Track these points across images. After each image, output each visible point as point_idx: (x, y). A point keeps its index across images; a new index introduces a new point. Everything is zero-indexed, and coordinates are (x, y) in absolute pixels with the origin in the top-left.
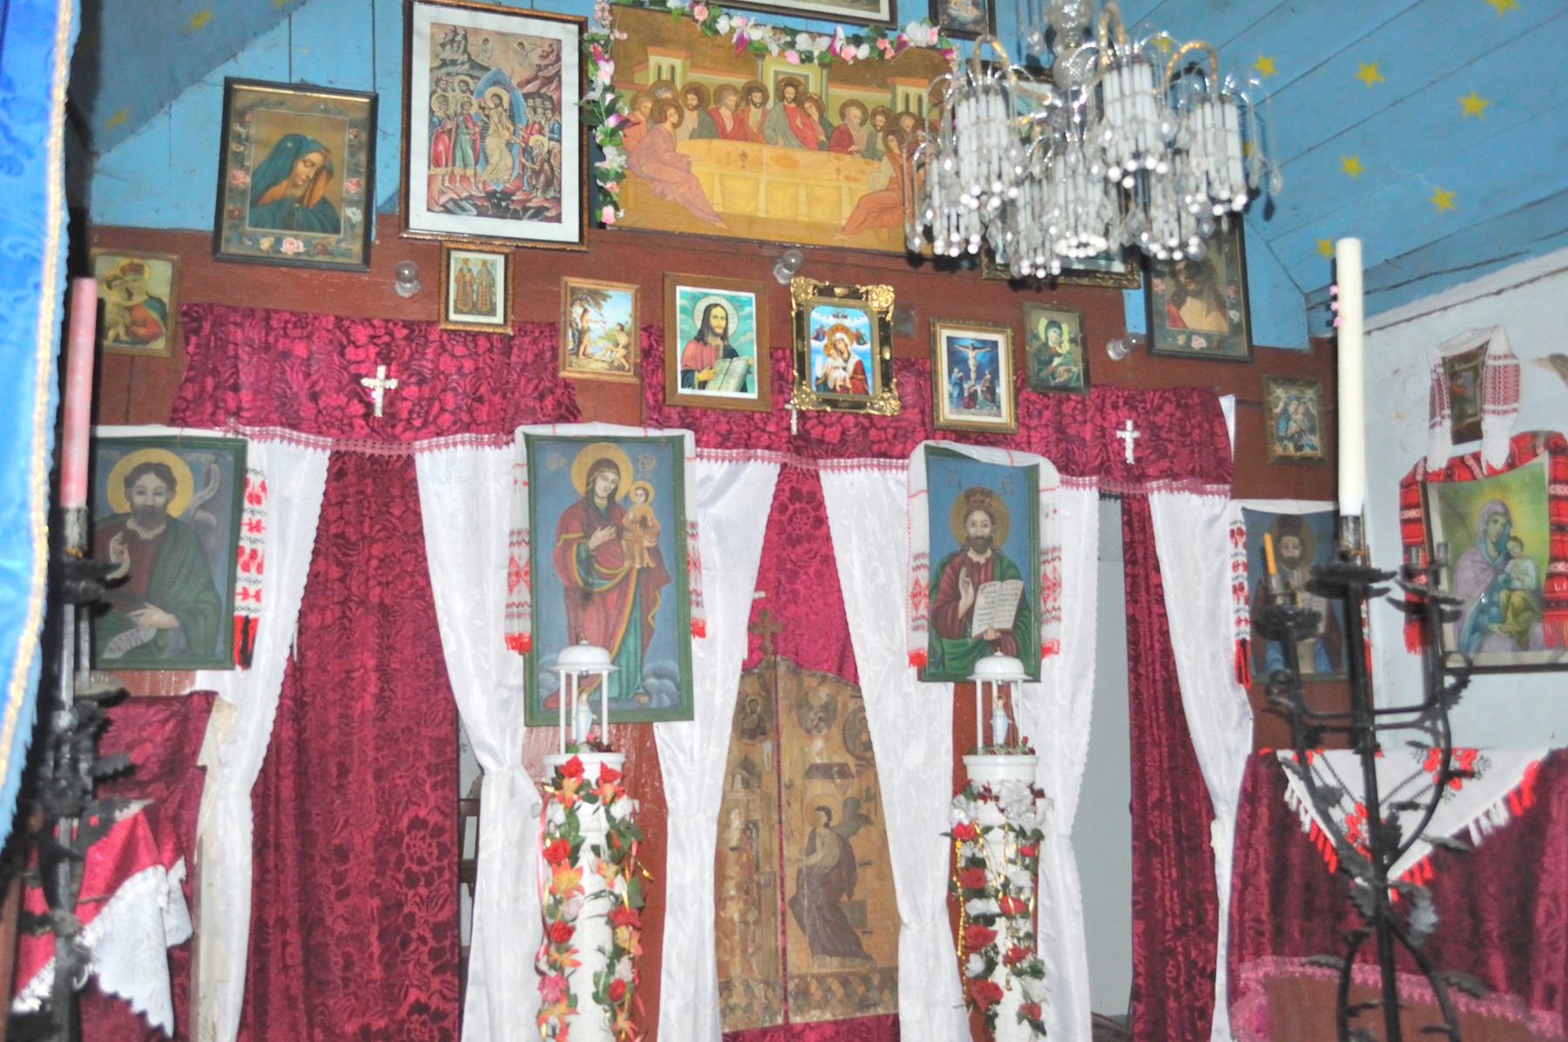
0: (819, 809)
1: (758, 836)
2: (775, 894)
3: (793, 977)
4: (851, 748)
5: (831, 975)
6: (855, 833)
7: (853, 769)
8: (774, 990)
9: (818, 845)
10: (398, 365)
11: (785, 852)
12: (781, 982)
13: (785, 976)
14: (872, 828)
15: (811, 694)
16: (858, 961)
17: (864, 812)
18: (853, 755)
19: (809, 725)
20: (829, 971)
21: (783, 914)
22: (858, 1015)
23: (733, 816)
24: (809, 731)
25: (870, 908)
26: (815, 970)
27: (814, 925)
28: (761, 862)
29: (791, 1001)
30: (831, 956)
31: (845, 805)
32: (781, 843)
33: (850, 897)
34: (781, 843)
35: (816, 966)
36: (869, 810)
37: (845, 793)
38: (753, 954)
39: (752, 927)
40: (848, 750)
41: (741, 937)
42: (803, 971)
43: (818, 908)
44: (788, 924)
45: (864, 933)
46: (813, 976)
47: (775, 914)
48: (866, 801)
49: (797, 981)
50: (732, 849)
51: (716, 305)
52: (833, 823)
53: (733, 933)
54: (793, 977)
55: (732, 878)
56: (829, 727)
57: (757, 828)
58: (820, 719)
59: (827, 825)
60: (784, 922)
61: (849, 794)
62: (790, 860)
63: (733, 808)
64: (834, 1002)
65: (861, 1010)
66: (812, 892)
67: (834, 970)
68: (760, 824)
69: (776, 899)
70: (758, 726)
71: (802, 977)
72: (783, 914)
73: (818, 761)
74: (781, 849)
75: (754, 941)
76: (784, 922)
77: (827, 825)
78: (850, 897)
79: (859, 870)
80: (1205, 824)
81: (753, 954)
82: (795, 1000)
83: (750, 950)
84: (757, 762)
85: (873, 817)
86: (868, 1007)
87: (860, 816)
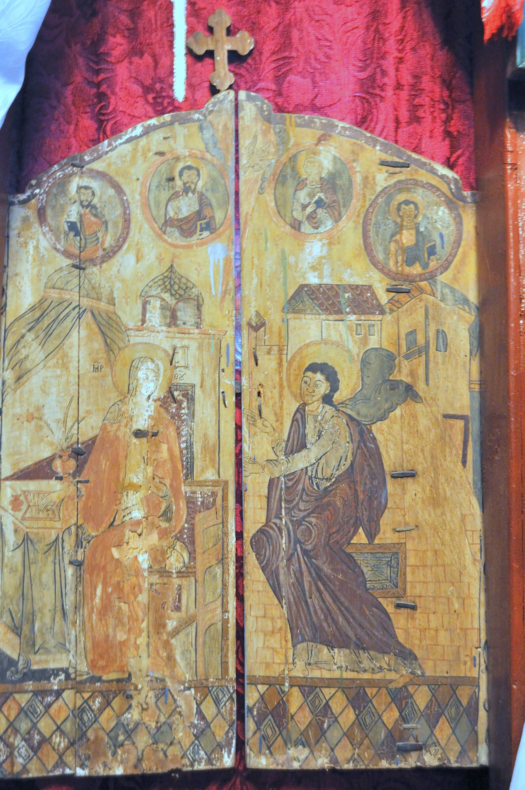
0: (313, 368)
1: (192, 415)
2: (224, 523)
3: (255, 682)
4: (381, 256)
5: (330, 683)
6: (382, 418)
7: (384, 298)
8: (217, 702)
9: (311, 437)
10: (203, 758)
11: (245, 447)
12: (232, 687)
13: (240, 675)
14: (419, 407)
15: (302, 158)
16: (385, 660)
17: (404, 377)
18: (383, 270)
19: (298, 215)
20: (327, 675)
21: (240, 560)
22: (384, 764)
23: (141, 374)
24: (296, 226)
25: (411, 560)
26: (299, 671)
27: (299, 582)
28: (198, 464)
29: (250, 725)
30: (331, 646)
31: (365, 363)
32: (238, 427)
33: (371, 536)
34: (238, 427)
35: (300, 664)
36: (412, 374)
37: (365, 341)
38: (176, 632)
39: (176, 582)
40: (374, 262)
41: (151, 598)
42: (275, 671)
43: (305, 552)
44: (248, 581)
45: (398, 606)
46: (294, 682)
47: (222, 561)
48: (407, 357)
49: (262, 688)
50: (139, 434)
51: (199, 175)
52: (337, 397)
53: (136, 589)
54: (255, 682)
55: (136, 488)
56: (337, 220)
57: (191, 399)
58: (319, 203)
59: (327, 399)
60: (240, 575)
61: (373, 342)
62: (254, 461)
63: (143, 359)
64: (334, 734)
65: (392, 757)
66: (297, 524)
67: (337, 674)
68: (198, 391)
69: (226, 534)
70: (199, 215)
71: (269, 682)
72: (240, 560)
73: (313, 280)
74: (239, 440)
75: (178, 609)
76: (240, 575)
77: (327, 399)
78: (371, 536)
79: (391, 486)
80: (515, 723)
81: (176, 632)
82: (258, 724)
83: (171, 625)
84: (194, 277)
85: (420, 387)
86: (405, 751)
87: (394, 385)
